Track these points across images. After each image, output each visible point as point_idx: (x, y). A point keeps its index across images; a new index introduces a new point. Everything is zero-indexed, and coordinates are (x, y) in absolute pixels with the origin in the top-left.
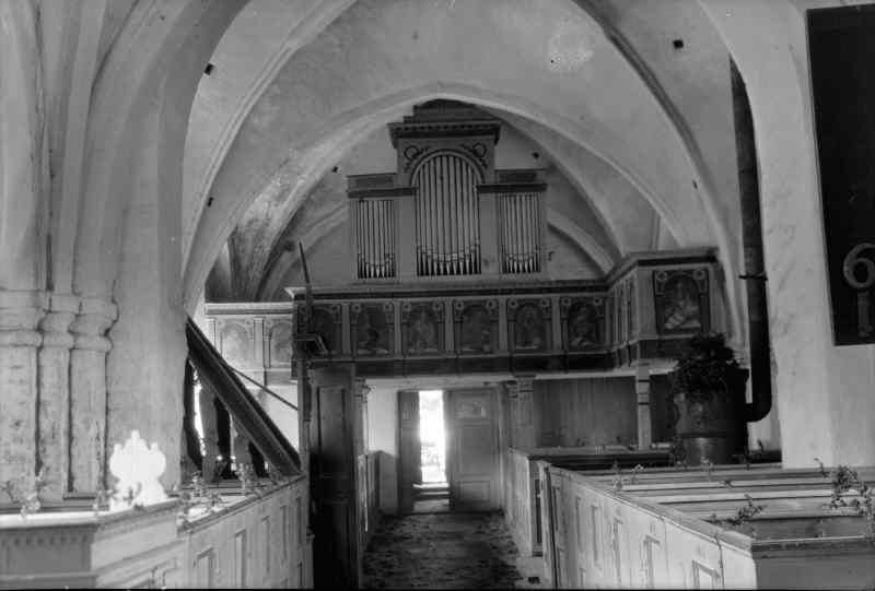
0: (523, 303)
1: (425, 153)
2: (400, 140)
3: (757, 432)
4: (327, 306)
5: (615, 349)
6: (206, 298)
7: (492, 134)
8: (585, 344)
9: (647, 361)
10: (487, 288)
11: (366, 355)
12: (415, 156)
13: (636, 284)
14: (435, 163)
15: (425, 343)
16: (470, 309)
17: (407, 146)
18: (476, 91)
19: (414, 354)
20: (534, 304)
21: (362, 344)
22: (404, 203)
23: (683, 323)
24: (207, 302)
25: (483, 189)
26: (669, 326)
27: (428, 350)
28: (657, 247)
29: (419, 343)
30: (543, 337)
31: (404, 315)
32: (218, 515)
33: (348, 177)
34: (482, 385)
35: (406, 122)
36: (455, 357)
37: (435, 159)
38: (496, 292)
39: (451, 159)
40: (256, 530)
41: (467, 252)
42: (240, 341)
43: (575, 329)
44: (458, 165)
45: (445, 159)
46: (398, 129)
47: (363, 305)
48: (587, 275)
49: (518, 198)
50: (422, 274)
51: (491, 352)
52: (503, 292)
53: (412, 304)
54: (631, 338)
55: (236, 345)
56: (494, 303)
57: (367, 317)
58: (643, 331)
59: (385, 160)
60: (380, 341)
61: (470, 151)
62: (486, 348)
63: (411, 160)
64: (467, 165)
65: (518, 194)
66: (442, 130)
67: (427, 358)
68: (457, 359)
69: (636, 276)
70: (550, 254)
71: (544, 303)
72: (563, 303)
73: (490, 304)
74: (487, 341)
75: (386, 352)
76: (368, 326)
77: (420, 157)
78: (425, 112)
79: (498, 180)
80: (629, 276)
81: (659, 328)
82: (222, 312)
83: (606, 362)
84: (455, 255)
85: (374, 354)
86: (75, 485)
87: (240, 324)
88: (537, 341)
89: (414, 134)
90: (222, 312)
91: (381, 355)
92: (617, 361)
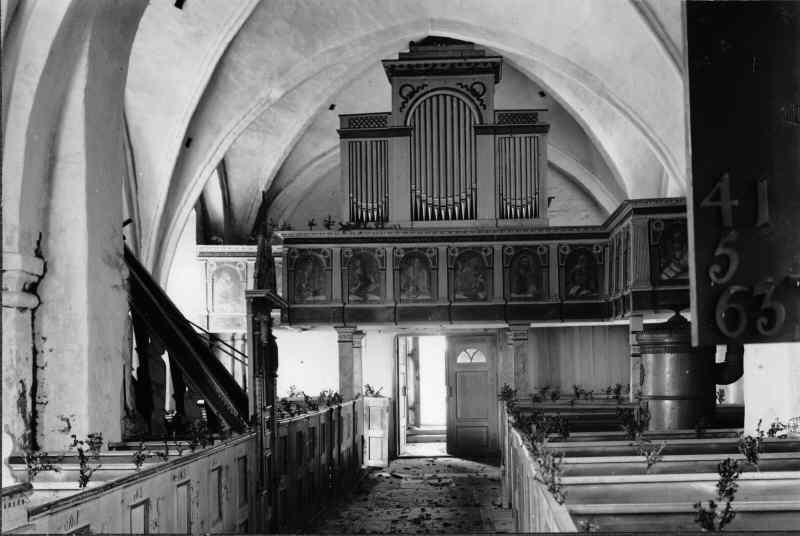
0: (356, 253)
1: (421, 92)
2: (395, 78)
3: (730, 394)
4: (319, 251)
5: (612, 299)
6: (197, 240)
7: (491, 72)
8: (584, 292)
9: (640, 313)
10: (453, 234)
11: (427, 301)
12: (411, 95)
13: (631, 232)
14: (431, 102)
15: (417, 289)
16: (466, 256)
17: (404, 83)
18: (468, 27)
19: (407, 301)
20: (586, 251)
21: (353, 289)
22: (398, 147)
23: (678, 274)
24: (198, 243)
25: (482, 130)
26: (664, 277)
27: (420, 298)
28: (666, 193)
29: (411, 288)
30: (539, 286)
31: (396, 260)
32: (145, 474)
33: (340, 116)
34: (482, 331)
35: (400, 59)
36: (447, 304)
37: (431, 98)
38: (491, 238)
39: (448, 98)
40: (191, 484)
41: (529, 200)
42: (232, 284)
43: (573, 279)
44: (455, 105)
45: (441, 99)
46: (393, 66)
47: (354, 250)
48: (593, 220)
49: (517, 140)
50: (416, 219)
51: (485, 300)
52: (500, 238)
53: (405, 249)
54: (626, 288)
55: (229, 288)
56: (545, 249)
57: (358, 263)
58: (637, 282)
59: (378, 97)
60: (372, 287)
61: (468, 90)
62: (481, 295)
63: (405, 97)
64: (465, 104)
65: (517, 136)
66: (439, 67)
67: (523, 303)
68: (505, 306)
69: (631, 223)
70: (550, 199)
71: (430, 252)
72: (561, 251)
73: (597, 249)
74: (482, 288)
75: (377, 298)
76: (358, 271)
77: (417, 95)
78: (421, 48)
79: (347, 126)
80: (625, 224)
81: (655, 279)
82: (213, 255)
83: (603, 312)
84: (450, 199)
85: (365, 301)
86: (39, 440)
87: (232, 266)
88: (532, 288)
89: (411, 72)
90: (213, 255)
91: (371, 302)
92: (614, 314)
